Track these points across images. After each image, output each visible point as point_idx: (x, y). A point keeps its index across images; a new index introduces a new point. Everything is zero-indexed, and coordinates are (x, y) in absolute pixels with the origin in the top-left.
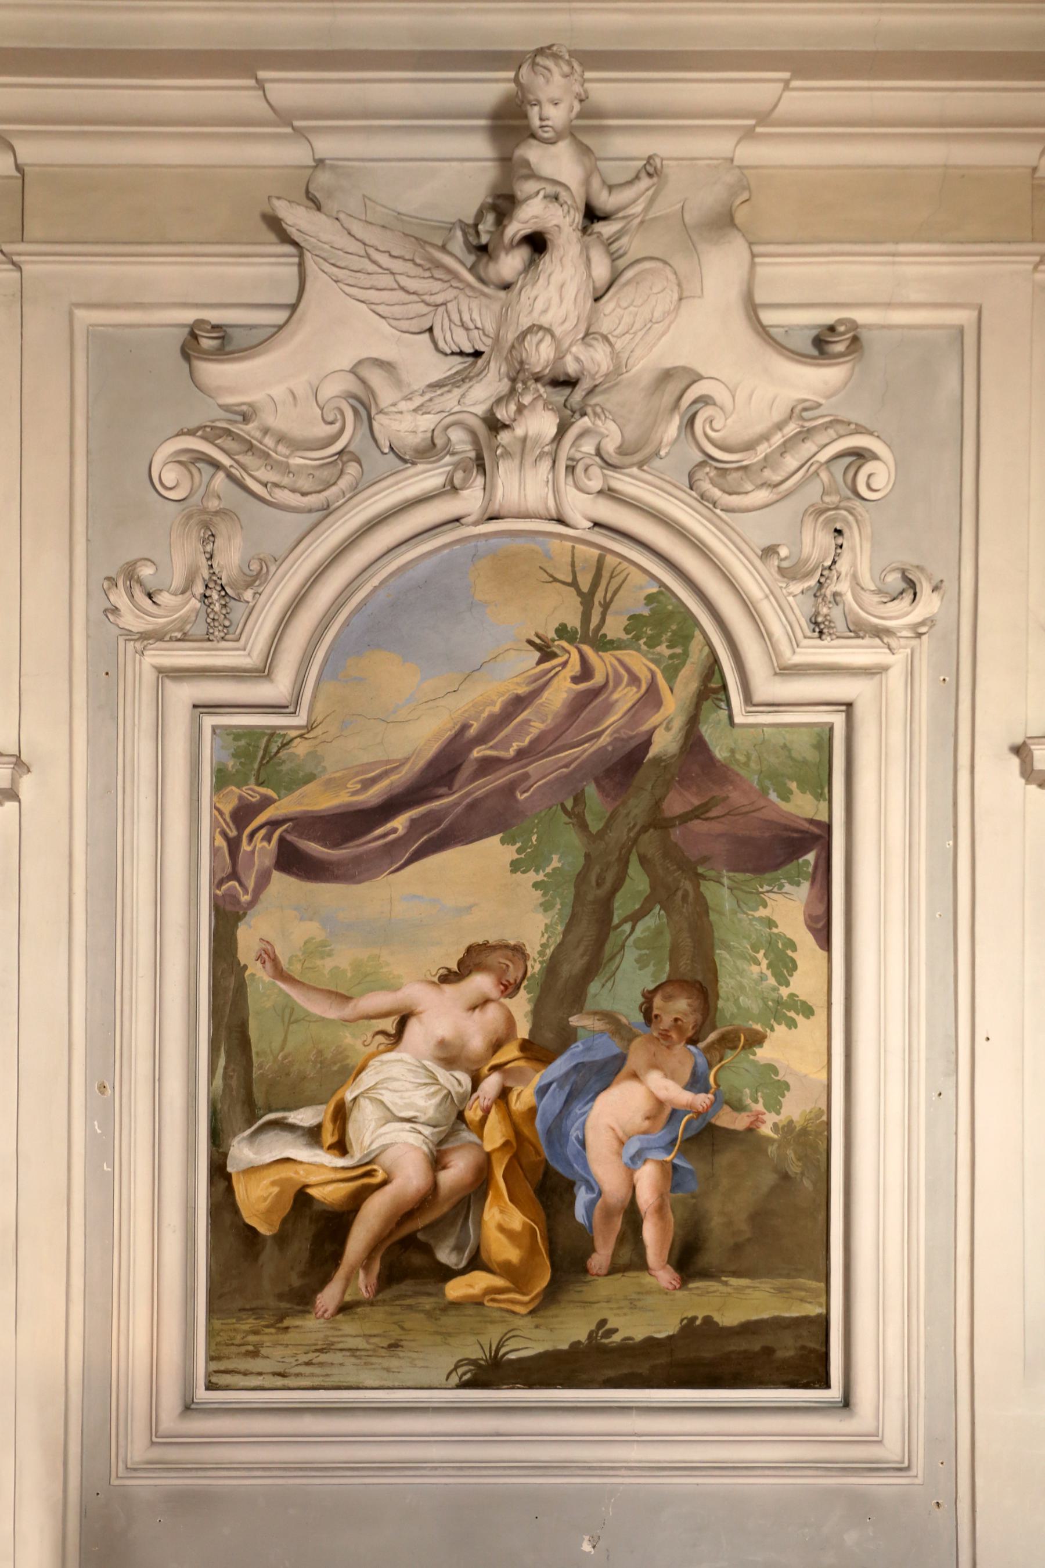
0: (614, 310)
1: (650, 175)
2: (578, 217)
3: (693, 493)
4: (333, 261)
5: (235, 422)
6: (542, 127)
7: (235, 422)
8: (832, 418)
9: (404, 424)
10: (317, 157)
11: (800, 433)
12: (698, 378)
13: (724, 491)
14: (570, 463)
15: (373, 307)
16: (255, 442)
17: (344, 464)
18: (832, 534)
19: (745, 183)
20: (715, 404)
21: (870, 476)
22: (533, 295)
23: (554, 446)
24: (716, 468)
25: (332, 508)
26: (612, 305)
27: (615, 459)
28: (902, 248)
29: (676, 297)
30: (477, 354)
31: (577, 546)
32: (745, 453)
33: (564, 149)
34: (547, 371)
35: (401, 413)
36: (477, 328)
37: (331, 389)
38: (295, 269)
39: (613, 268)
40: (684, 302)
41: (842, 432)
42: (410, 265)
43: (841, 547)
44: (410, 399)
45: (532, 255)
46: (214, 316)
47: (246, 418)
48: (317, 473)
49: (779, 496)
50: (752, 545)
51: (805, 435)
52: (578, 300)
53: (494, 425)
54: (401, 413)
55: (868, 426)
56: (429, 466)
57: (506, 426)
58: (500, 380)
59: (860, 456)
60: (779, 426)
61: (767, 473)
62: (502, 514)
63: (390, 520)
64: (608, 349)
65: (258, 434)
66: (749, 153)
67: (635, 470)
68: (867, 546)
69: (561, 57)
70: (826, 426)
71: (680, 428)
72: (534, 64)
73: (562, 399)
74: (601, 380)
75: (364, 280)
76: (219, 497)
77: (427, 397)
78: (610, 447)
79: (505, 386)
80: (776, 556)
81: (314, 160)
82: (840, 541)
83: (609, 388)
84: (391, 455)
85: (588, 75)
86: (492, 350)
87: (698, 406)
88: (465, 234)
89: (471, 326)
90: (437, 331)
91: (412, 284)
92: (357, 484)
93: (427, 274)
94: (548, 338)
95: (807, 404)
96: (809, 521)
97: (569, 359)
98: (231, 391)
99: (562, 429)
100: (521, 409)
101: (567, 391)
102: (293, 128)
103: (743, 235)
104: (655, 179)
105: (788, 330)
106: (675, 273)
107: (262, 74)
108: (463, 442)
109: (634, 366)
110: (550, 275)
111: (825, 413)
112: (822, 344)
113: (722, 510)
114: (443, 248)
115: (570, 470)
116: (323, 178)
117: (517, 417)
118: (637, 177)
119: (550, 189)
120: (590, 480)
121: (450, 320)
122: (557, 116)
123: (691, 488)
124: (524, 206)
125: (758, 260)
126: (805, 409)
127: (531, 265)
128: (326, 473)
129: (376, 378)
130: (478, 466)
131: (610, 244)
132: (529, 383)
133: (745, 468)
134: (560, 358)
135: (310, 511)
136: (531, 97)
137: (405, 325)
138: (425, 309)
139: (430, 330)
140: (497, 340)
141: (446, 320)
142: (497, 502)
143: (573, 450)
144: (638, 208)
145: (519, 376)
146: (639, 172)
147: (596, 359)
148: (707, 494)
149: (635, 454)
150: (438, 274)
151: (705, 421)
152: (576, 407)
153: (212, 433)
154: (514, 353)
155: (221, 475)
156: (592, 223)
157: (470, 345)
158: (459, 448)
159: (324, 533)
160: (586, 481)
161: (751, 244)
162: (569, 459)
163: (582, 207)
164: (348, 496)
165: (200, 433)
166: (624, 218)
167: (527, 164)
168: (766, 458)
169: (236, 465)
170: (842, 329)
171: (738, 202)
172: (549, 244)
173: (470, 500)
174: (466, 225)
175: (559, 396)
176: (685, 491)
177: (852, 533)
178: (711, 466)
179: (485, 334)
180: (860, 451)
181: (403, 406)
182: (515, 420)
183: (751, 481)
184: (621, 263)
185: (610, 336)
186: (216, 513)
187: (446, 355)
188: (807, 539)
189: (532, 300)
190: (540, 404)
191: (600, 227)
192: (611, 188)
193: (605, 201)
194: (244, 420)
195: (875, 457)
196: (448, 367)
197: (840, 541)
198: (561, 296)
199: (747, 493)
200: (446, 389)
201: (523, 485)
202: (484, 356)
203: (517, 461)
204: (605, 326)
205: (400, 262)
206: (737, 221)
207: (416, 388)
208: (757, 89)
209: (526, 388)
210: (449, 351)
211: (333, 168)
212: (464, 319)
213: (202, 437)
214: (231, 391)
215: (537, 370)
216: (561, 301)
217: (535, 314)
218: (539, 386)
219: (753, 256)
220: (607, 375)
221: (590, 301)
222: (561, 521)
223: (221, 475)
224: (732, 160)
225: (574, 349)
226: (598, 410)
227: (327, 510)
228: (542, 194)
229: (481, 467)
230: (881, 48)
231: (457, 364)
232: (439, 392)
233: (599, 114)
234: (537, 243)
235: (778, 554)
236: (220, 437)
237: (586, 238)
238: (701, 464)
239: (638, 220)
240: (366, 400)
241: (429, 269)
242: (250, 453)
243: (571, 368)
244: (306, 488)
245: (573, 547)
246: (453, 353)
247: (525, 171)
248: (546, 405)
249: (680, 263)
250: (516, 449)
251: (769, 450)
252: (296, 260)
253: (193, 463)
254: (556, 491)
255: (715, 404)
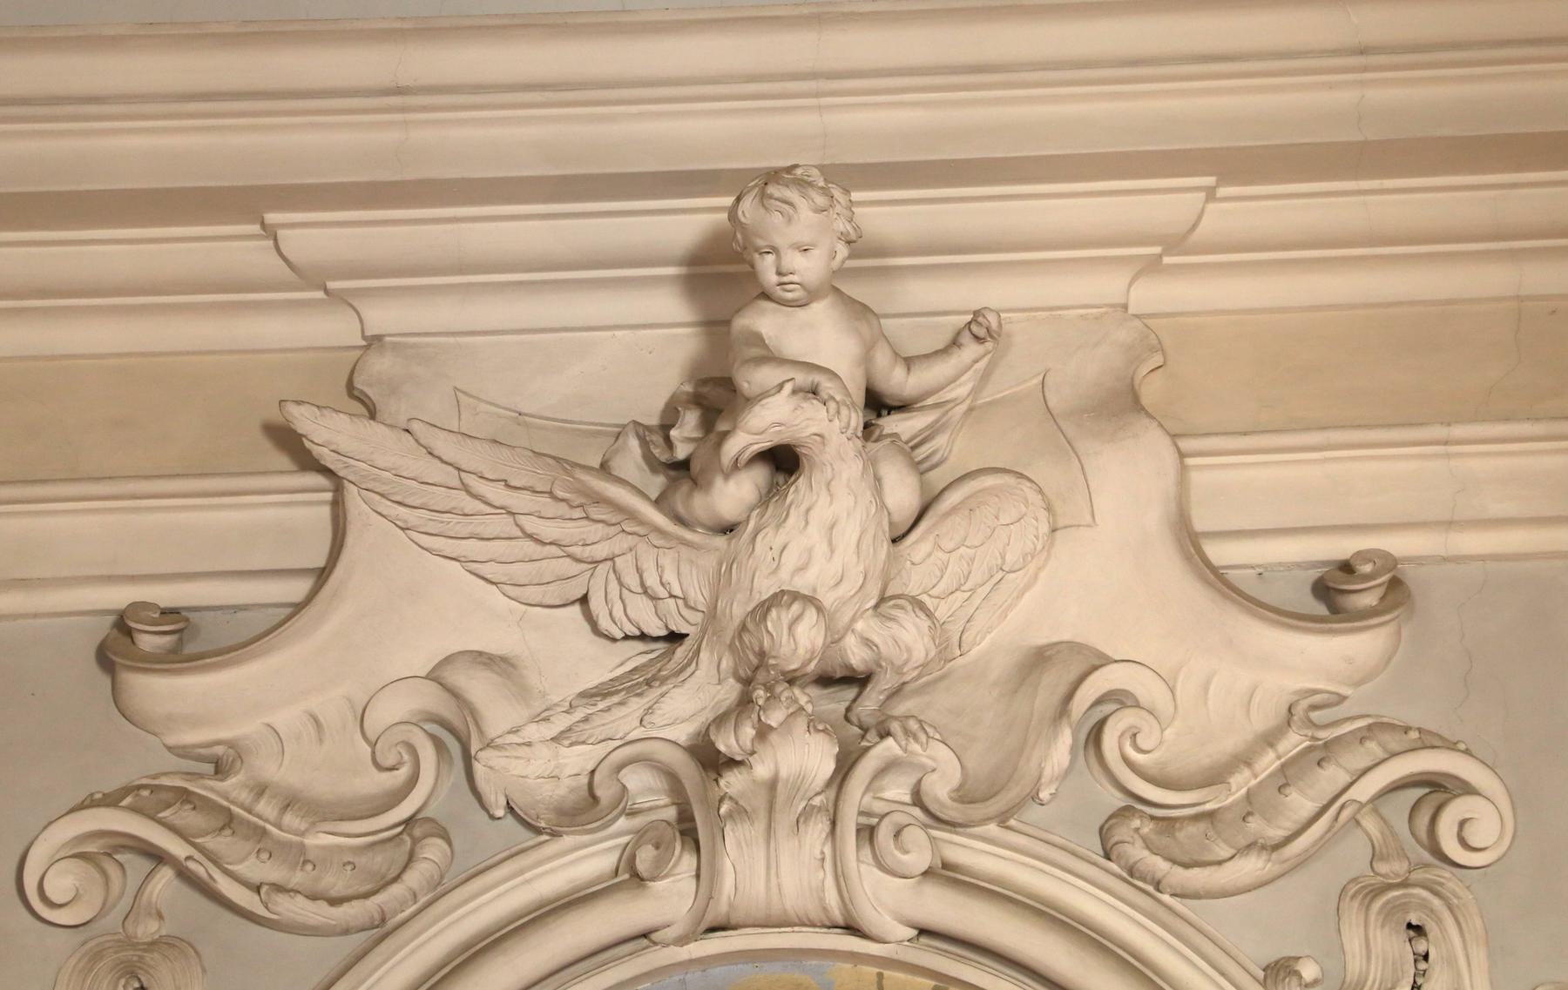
0: (929, 555)
1: (977, 338)
2: (856, 419)
3: (1113, 866)
4: (398, 498)
5: (201, 776)
6: (781, 284)
7: (201, 776)
8: (1370, 721)
9: (537, 766)
10: (368, 333)
11: (1309, 749)
12: (1101, 661)
13: (1174, 862)
14: (864, 820)
15: (473, 566)
16: (236, 810)
17: (415, 841)
18: (1405, 934)
19: (1153, 340)
20: (1137, 705)
21: (1462, 824)
22: (778, 543)
23: (832, 793)
24: (1153, 818)
25: (391, 924)
26: (925, 547)
27: (953, 812)
28: (1459, 431)
29: (1044, 528)
30: (675, 638)
31: (887, 973)
32: (1205, 791)
33: (821, 310)
34: (812, 666)
35: (529, 744)
36: (672, 596)
37: (389, 711)
38: (326, 511)
39: (923, 486)
40: (1058, 534)
41: (1394, 746)
42: (546, 500)
43: (1426, 957)
44: (546, 719)
45: (773, 477)
46: (165, 595)
47: (221, 769)
48: (362, 861)
49: (1286, 866)
50: (1242, 958)
51: (1322, 753)
52: (864, 547)
53: (711, 760)
54: (529, 744)
55: (1446, 734)
56: (586, 838)
57: (732, 763)
58: (720, 682)
59: (1439, 788)
60: (1269, 739)
61: (1255, 824)
62: (733, 922)
63: (507, 944)
64: (925, 623)
65: (245, 796)
66: (1152, 295)
67: (992, 829)
68: (1479, 955)
69: (810, 184)
70: (1363, 736)
71: (1073, 750)
72: (763, 197)
73: (842, 707)
74: (915, 673)
75: (455, 524)
76: (160, 916)
77: (579, 714)
78: (940, 789)
79: (729, 692)
80: (1295, 980)
81: (364, 337)
82: (1421, 946)
83: (928, 684)
84: (510, 820)
85: (856, 196)
86: (704, 631)
87: (1108, 708)
88: (644, 443)
89: (662, 593)
90: (596, 604)
91: (548, 530)
92: (442, 877)
93: (578, 513)
94: (811, 614)
95: (1317, 699)
96: (1352, 911)
97: (851, 642)
98: (195, 721)
99: (846, 765)
100: (763, 732)
101: (851, 693)
102: (326, 291)
103: (1161, 425)
104: (989, 345)
105: (1263, 572)
106: (1041, 491)
107: (272, 217)
108: (651, 791)
109: (974, 644)
110: (808, 510)
111: (1355, 711)
112: (1333, 594)
113: (1173, 895)
114: (604, 468)
115: (866, 834)
116: (380, 365)
117: (758, 747)
118: (955, 343)
119: (802, 378)
120: (906, 852)
121: (621, 584)
122: (808, 267)
123: (1108, 857)
124: (757, 409)
125: (1190, 461)
126: (1314, 707)
127: (770, 495)
128: (379, 859)
129: (478, 687)
130: (682, 833)
131: (913, 448)
132: (779, 689)
133: (1210, 816)
134: (834, 640)
135: (346, 932)
136: (760, 242)
137: (533, 593)
138: (576, 568)
139: (584, 600)
140: (712, 615)
141: (614, 586)
142: (724, 899)
143: (867, 798)
144: (961, 390)
145: (756, 679)
146: (959, 333)
147: (907, 638)
148: (1140, 866)
149: (991, 798)
150: (595, 512)
151: (1122, 735)
152: (869, 721)
153: (151, 798)
154: (746, 638)
155: (166, 874)
156: (879, 416)
157: (660, 624)
158: (643, 801)
159: (376, 969)
160: (897, 853)
161: (1174, 437)
162: (861, 813)
163: (859, 397)
164: (423, 900)
165: (127, 801)
166: (937, 405)
167: (757, 339)
168: (1249, 797)
169: (197, 855)
170: (1367, 568)
171: (1144, 370)
172: (804, 460)
173: (671, 897)
174: (648, 428)
175: (834, 702)
176: (1095, 864)
177: (1443, 930)
178: (1142, 815)
179: (687, 606)
180: (1434, 778)
181: (533, 732)
182: (753, 753)
183: (1225, 841)
184: (938, 478)
185: (924, 598)
186: (153, 945)
187: (614, 640)
188: (1353, 941)
189: (776, 553)
190: (801, 723)
191: (893, 424)
192: (909, 362)
193: (898, 382)
194: (217, 772)
195: (1467, 789)
196: (618, 661)
197: (1421, 946)
198: (830, 543)
199: (1220, 863)
200: (616, 699)
201: (776, 868)
202: (688, 642)
203: (761, 825)
204: (914, 581)
205: (526, 496)
206: (1145, 401)
207: (556, 699)
208: (1164, 204)
209: (773, 697)
210: (619, 635)
211: (396, 347)
212: (648, 583)
213: (133, 809)
214: (195, 721)
215: (793, 667)
216: (832, 551)
217: (784, 574)
218: (797, 691)
219: (1182, 455)
220: (924, 665)
221: (885, 546)
222: (852, 929)
223: (166, 874)
224: (1125, 307)
225: (859, 626)
226: (913, 725)
227: (382, 930)
228: (788, 387)
229: (687, 830)
230: (1371, 136)
231: (634, 656)
232: (601, 705)
233: (881, 251)
234: (783, 461)
235: (1298, 974)
236: (169, 806)
237: (870, 445)
238: (1123, 813)
239: (964, 407)
240: (457, 723)
241: (581, 506)
242: (228, 832)
243: (857, 657)
244: (338, 890)
245: (880, 976)
246: (627, 637)
247: (755, 352)
248: (811, 726)
249: (1045, 472)
250: (760, 802)
251: (1253, 782)
252: (329, 496)
253: (109, 855)
254: (840, 877)
255: (1137, 705)
